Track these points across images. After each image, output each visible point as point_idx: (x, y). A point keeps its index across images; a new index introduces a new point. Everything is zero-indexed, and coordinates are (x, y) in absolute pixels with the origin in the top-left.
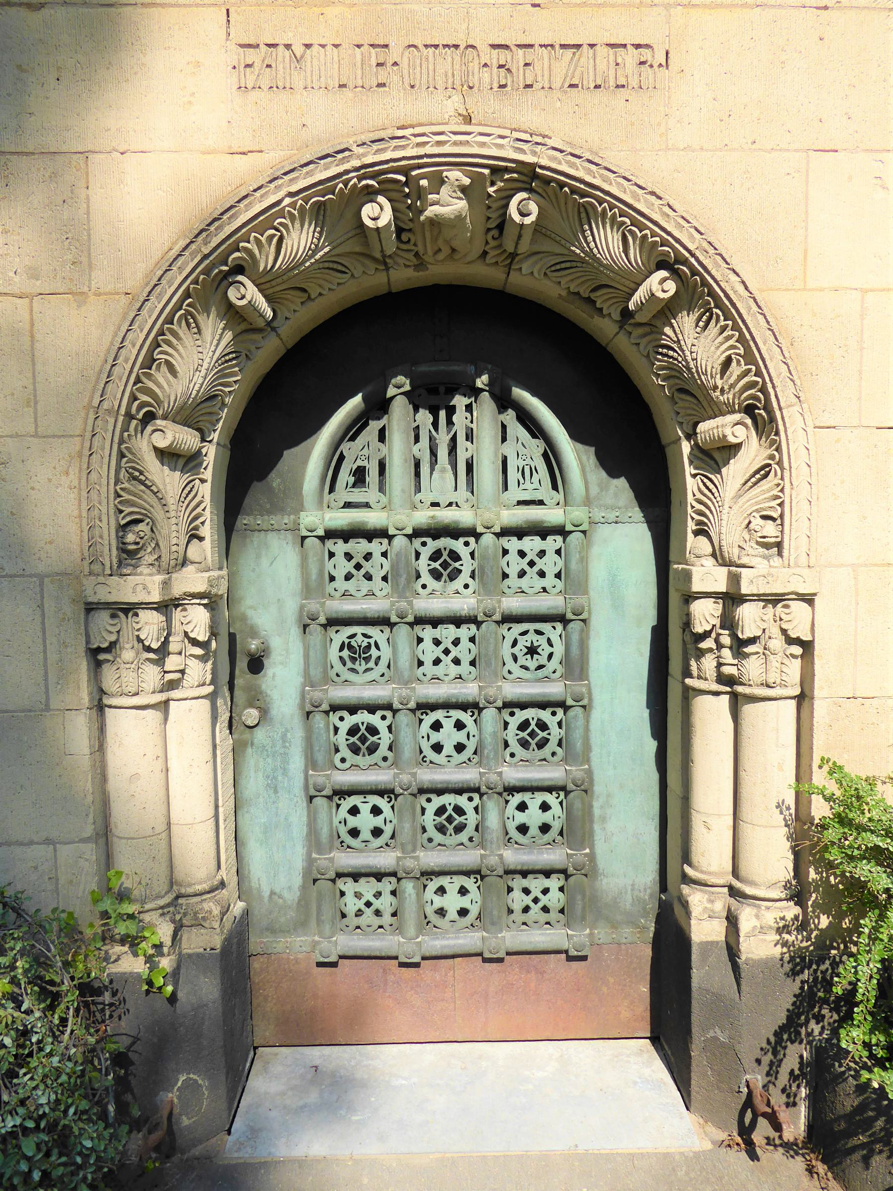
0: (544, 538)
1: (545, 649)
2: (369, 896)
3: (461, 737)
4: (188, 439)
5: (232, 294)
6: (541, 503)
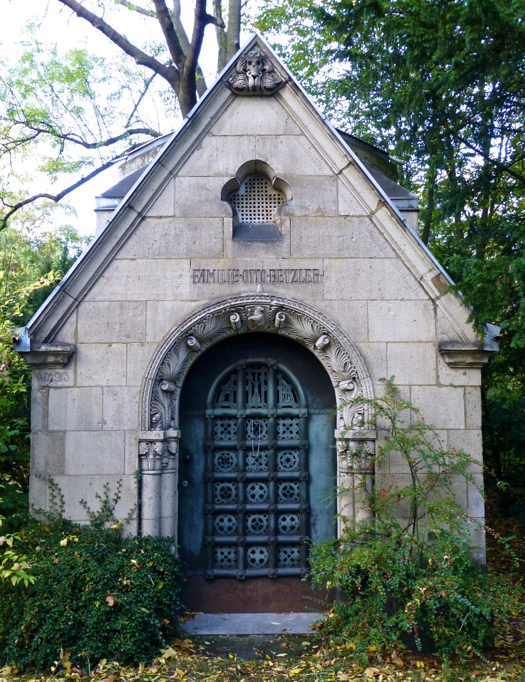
0: (292, 419)
1: (293, 460)
2: (226, 554)
3: (261, 492)
4: (173, 387)
5: (189, 342)
6: (291, 407)
